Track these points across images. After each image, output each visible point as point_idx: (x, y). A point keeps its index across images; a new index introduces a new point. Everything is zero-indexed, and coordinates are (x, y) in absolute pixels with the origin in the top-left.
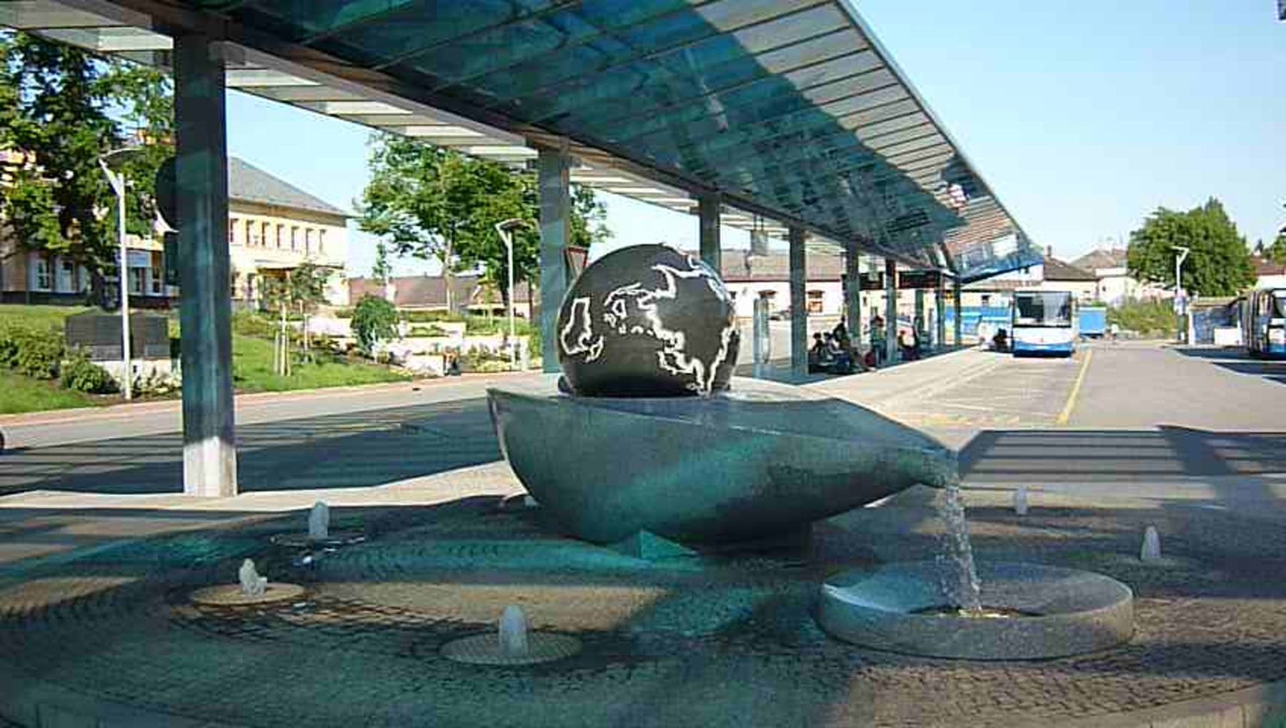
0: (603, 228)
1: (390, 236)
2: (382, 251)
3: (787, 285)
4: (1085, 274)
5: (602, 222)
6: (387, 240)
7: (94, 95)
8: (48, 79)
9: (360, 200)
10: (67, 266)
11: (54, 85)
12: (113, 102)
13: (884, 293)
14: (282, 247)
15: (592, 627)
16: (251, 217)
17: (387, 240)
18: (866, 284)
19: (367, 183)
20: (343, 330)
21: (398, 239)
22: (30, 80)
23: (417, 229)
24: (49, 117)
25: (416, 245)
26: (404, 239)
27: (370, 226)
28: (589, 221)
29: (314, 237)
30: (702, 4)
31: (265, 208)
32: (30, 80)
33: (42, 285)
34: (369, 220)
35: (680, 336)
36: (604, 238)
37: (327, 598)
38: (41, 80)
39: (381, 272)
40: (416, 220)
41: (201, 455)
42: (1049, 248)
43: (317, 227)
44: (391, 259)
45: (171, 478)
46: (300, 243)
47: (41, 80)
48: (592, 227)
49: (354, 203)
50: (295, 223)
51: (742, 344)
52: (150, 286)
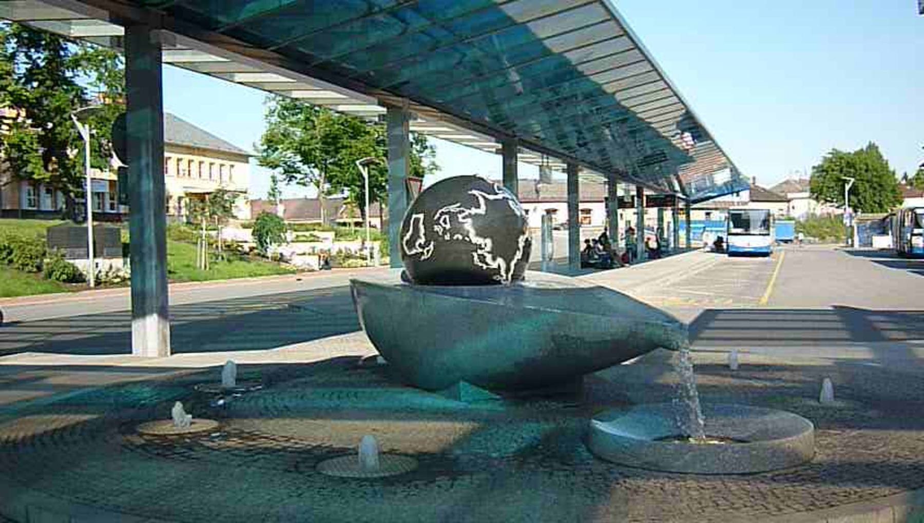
0: (433, 164)
1: (280, 170)
2: (274, 180)
3: (566, 205)
4: (780, 197)
5: (432, 159)
6: (278, 172)
7: (67, 68)
8: (34, 57)
9: (258, 143)
10: (48, 191)
11: (39, 61)
12: (81, 74)
13: (635, 210)
14: (203, 177)
15: (425, 451)
16: (180, 156)
17: (278, 172)
18: (622, 204)
19: (264, 132)
20: (247, 237)
21: (286, 172)
22: (21, 57)
23: (300, 164)
24: (35, 84)
25: (299, 176)
26: (291, 172)
27: (266, 163)
28: (423, 159)
29: (226, 170)
30: (504, 3)
31: (191, 150)
32: (21, 57)
33: (30, 205)
34: (265, 158)
35: (489, 241)
36: (434, 171)
38: (29, 57)
39: (274, 195)
40: (299, 158)
41: (144, 327)
42: (754, 178)
43: (228, 163)
44: (281, 186)
46: (215, 175)
47: (29, 57)
48: (425, 163)
49: (254, 146)
50: (212, 160)
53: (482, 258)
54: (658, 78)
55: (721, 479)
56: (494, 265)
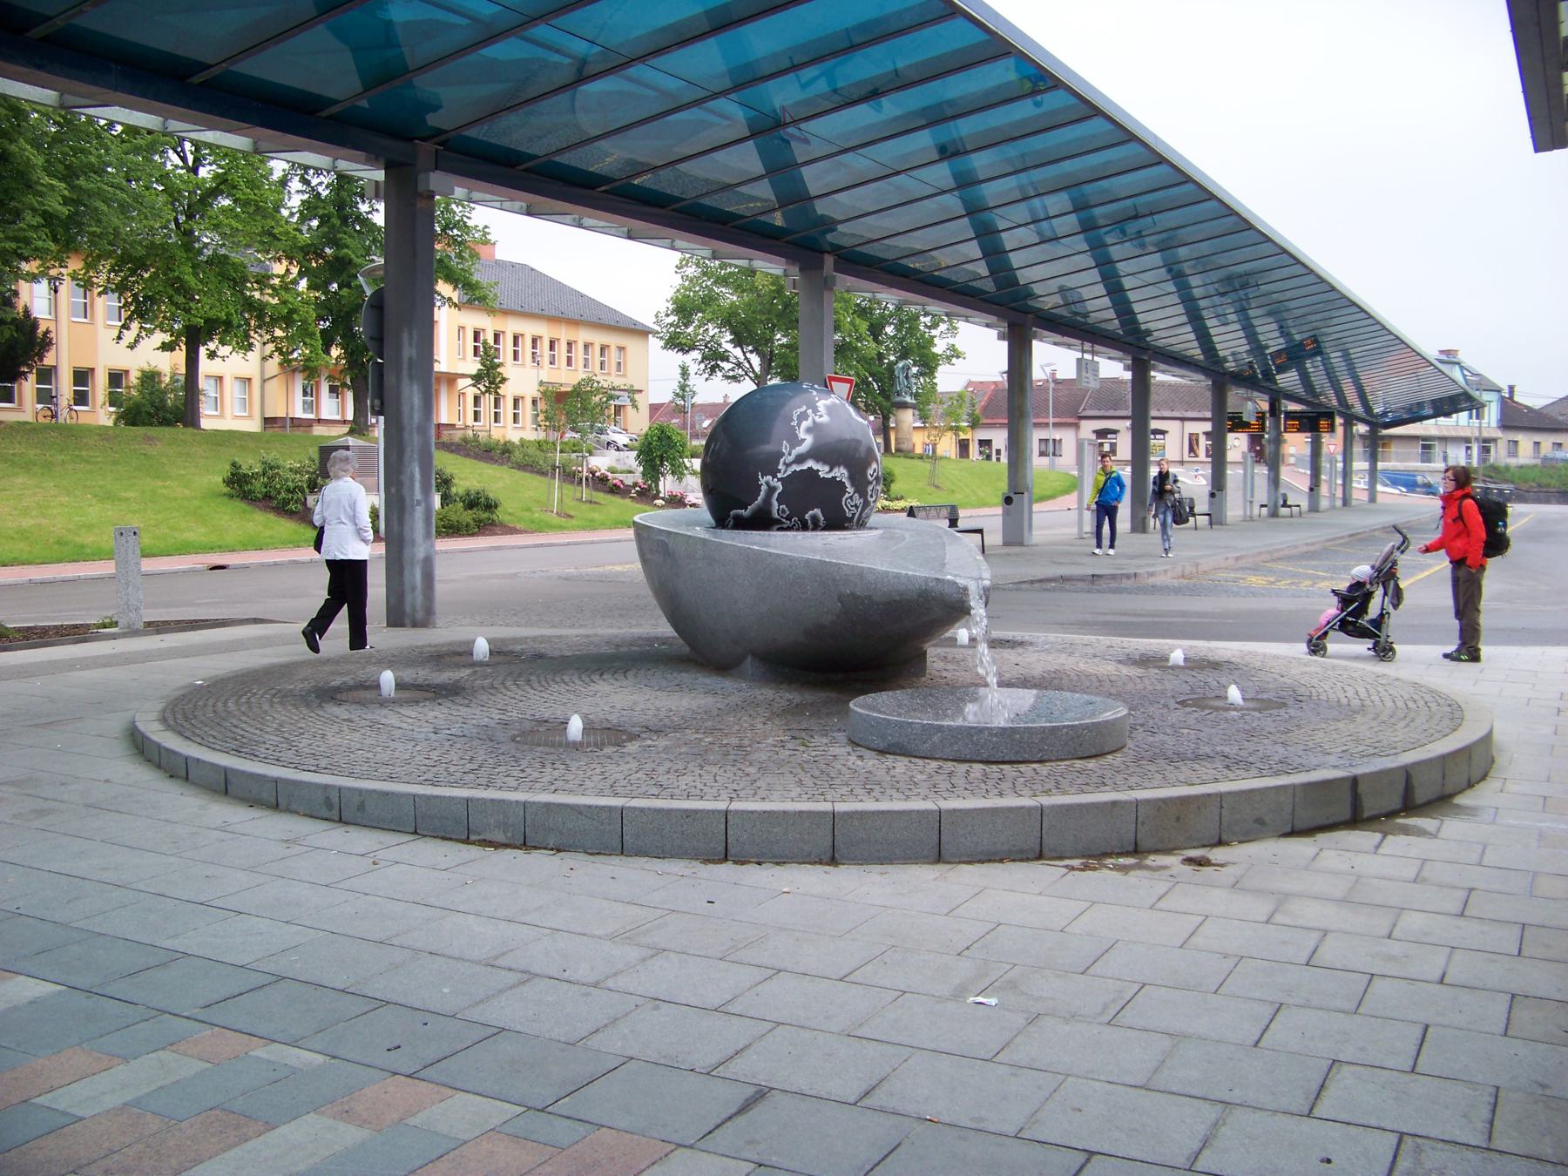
0: (952, 348)
1: (696, 355)
2: (685, 372)
4: (1560, 422)
5: (951, 341)
6: (692, 359)
7: (362, 197)
8: (314, 182)
10: (333, 389)
11: (320, 189)
17: (692, 359)
18: (1238, 424)
19: (670, 293)
20: (628, 466)
21: (704, 358)
22: (295, 184)
23: (729, 347)
24: (315, 223)
25: (726, 366)
26: (713, 359)
27: (676, 343)
28: (936, 340)
32: (295, 184)
33: (305, 411)
36: (954, 360)
37: (303, 680)
38: (307, 183)
39: (683, 398)
40: (729, 337)
42: (1511, 388)
44: (697, 382)
45: (400, 686)
47: (307, 183)
48: (939, 347)
51: (1428, 543)
52: (470, 416)
53: (803, 417)
54: (1061, 1078)
55: (795, 197)
56: (802, 435)
